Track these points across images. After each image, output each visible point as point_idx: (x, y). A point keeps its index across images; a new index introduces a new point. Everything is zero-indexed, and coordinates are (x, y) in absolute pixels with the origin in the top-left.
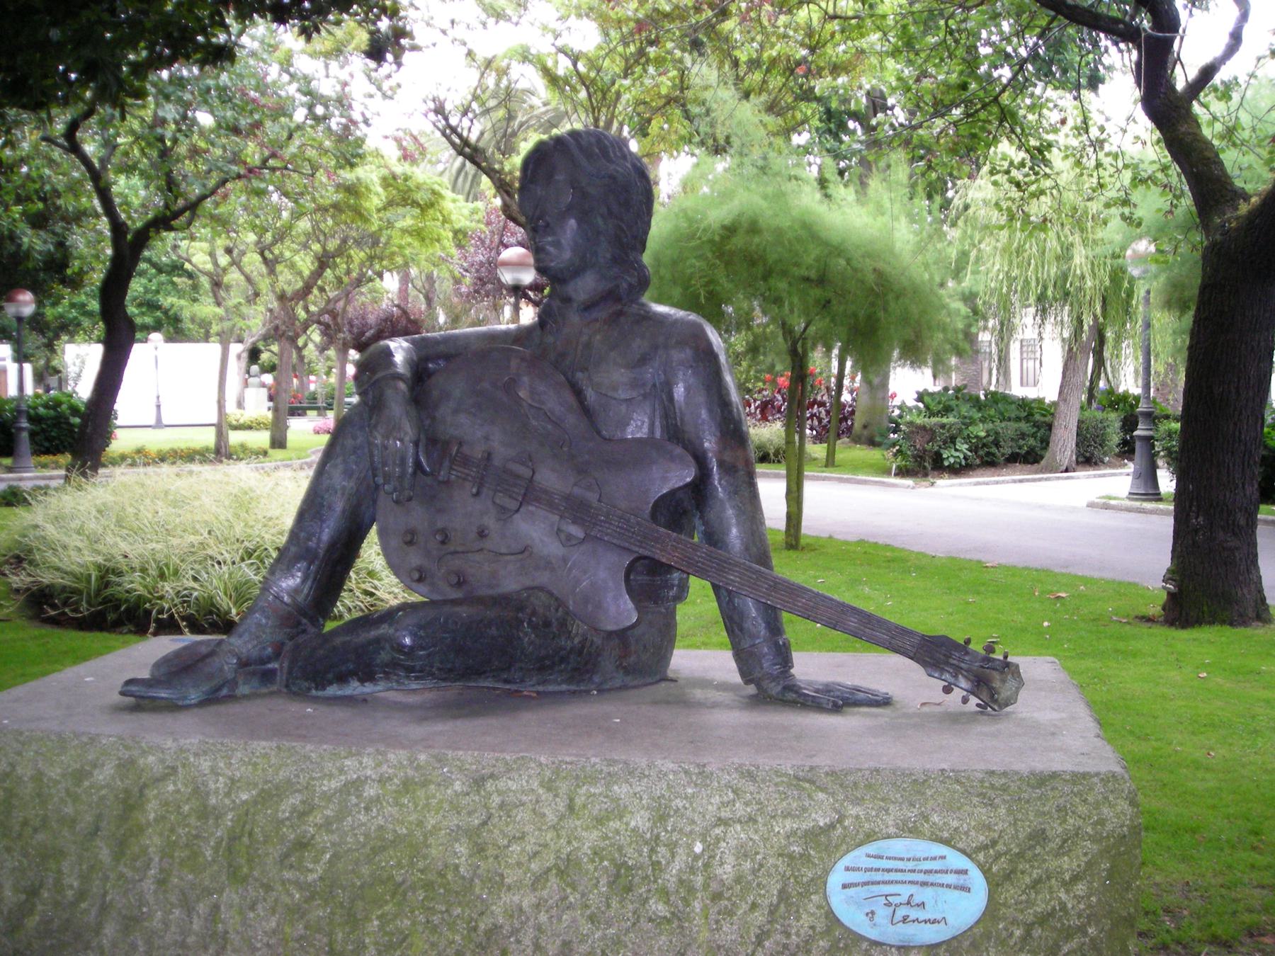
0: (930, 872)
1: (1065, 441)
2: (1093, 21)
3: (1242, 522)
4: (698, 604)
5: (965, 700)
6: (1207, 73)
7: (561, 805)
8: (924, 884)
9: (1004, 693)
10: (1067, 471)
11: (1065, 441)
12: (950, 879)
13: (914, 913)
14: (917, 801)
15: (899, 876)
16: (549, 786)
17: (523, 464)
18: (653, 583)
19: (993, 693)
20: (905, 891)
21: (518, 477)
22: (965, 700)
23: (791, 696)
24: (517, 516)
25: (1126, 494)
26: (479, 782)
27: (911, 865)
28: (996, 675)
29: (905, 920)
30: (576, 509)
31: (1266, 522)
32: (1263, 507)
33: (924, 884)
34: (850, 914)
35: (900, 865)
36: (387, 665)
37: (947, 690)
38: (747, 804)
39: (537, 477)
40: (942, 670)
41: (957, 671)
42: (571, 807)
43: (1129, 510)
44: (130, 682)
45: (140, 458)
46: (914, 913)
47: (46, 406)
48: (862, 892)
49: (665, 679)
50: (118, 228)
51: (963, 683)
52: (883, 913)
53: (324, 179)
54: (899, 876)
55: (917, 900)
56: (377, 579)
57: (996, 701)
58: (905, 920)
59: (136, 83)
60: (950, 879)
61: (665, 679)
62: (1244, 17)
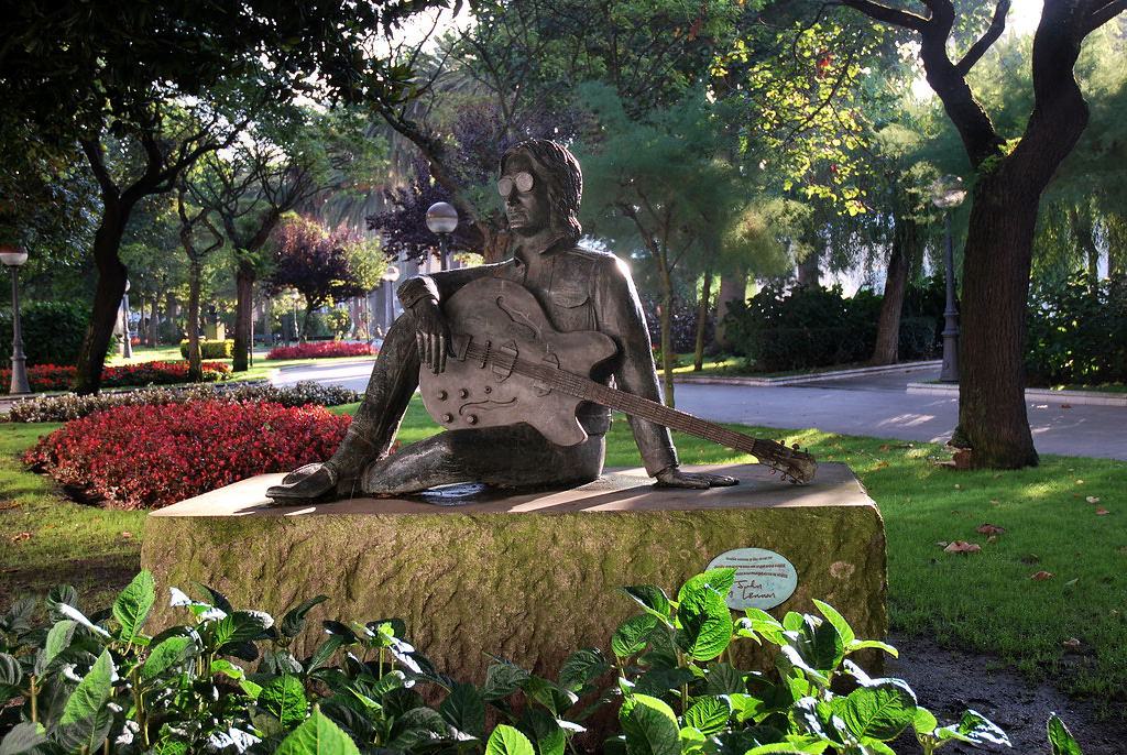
0: (761, 567)
1: (890, 336)
2: (893, 17)
8: (760, 574)
11: (890, 336)
15: (746, 570)
20: (750, 578)
27: (752, 563)
29: (750, 596)
30: (547, 375)
32: (1027, 390)
33: (760, 574)
35: (745, 563)
41: (778, 461)
47: (64, 310)
50: (110, 192)
53: (1104, 291)
54: (746, 570)
55: (756, 584)
58: (750, 596)
59: (90, 331)
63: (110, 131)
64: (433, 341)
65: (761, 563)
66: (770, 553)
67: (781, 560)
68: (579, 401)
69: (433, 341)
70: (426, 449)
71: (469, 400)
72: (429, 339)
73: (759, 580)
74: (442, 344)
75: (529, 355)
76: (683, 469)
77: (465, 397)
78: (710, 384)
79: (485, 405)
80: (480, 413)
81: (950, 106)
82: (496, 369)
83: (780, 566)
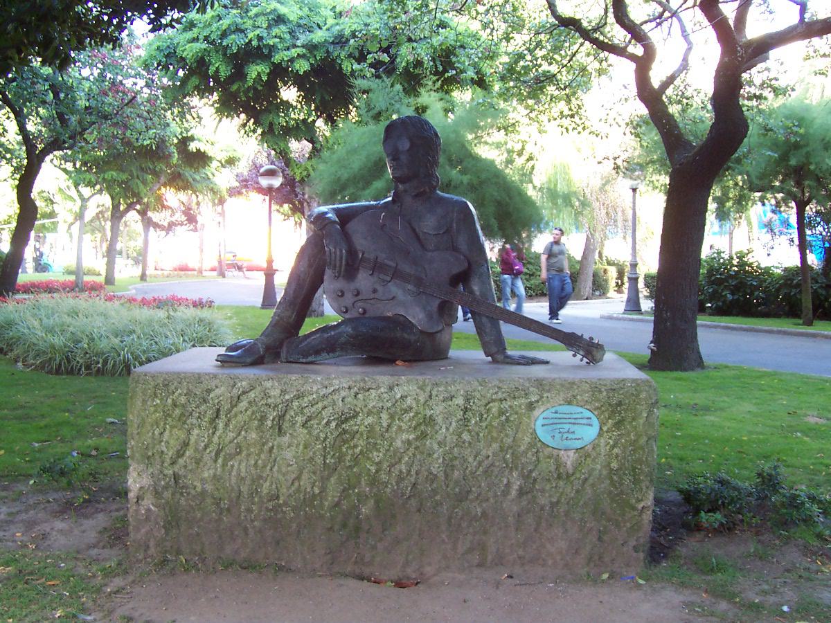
3: (690, 316)
4: (463, 324)
5: (582, 360)
6: (671, 80)
7: (427, 395)
9: (598, 356)
10: (587, 299)
12: (585, 421)
13: (570, 436)
14: (570, 392)
16: (421, 388)
17: (392, 260)
18: (445, 312)
19: (593, 356)
20: (567, 426)
21: (390, 266)
22: (582, 360)
23: (509, 360)
24: (390, 284)
25: (622, 311)
26: (391, 388)
28: (595, 349)
29: (567, 439)
31: (702, 326)
34: (542, 434)
35: (565, 416)
36: (344, 344)
37: (574, 356)
38: (503, 393)
39: (399, 267)
40: (572, 347)
42: (430, 397)
43: (624, 319)
44: (218, 356)
45: (30, 288)
46: (570, 436)
48: (550, 428)
49: (447, 358)
51: (581, 353)
52: (558, 436)
55: (571, 430)
56: (328, 312)
57: (595, 360)
58: (567, 439)
60: (585, 421)
61: (447, 358)
62: (689, 49)
63: (330, 120)
64: (338, 253)
65: (575, 416)
66: (580, 410)
67: (588, 414)
68: (440, 300)
69: (338, 253)
70: (334, 330)
71: (360, 297)
72: (335, 253)
73: (573, 428)
74: (344, 258)
75: (407, 268)
76: (509, 352)
77: (357, 295)
78: (779, 332)
79: (372, 301)
80: (368, 306)
81: (653, 114)
82: (382, 276)
83: (588, 418)
